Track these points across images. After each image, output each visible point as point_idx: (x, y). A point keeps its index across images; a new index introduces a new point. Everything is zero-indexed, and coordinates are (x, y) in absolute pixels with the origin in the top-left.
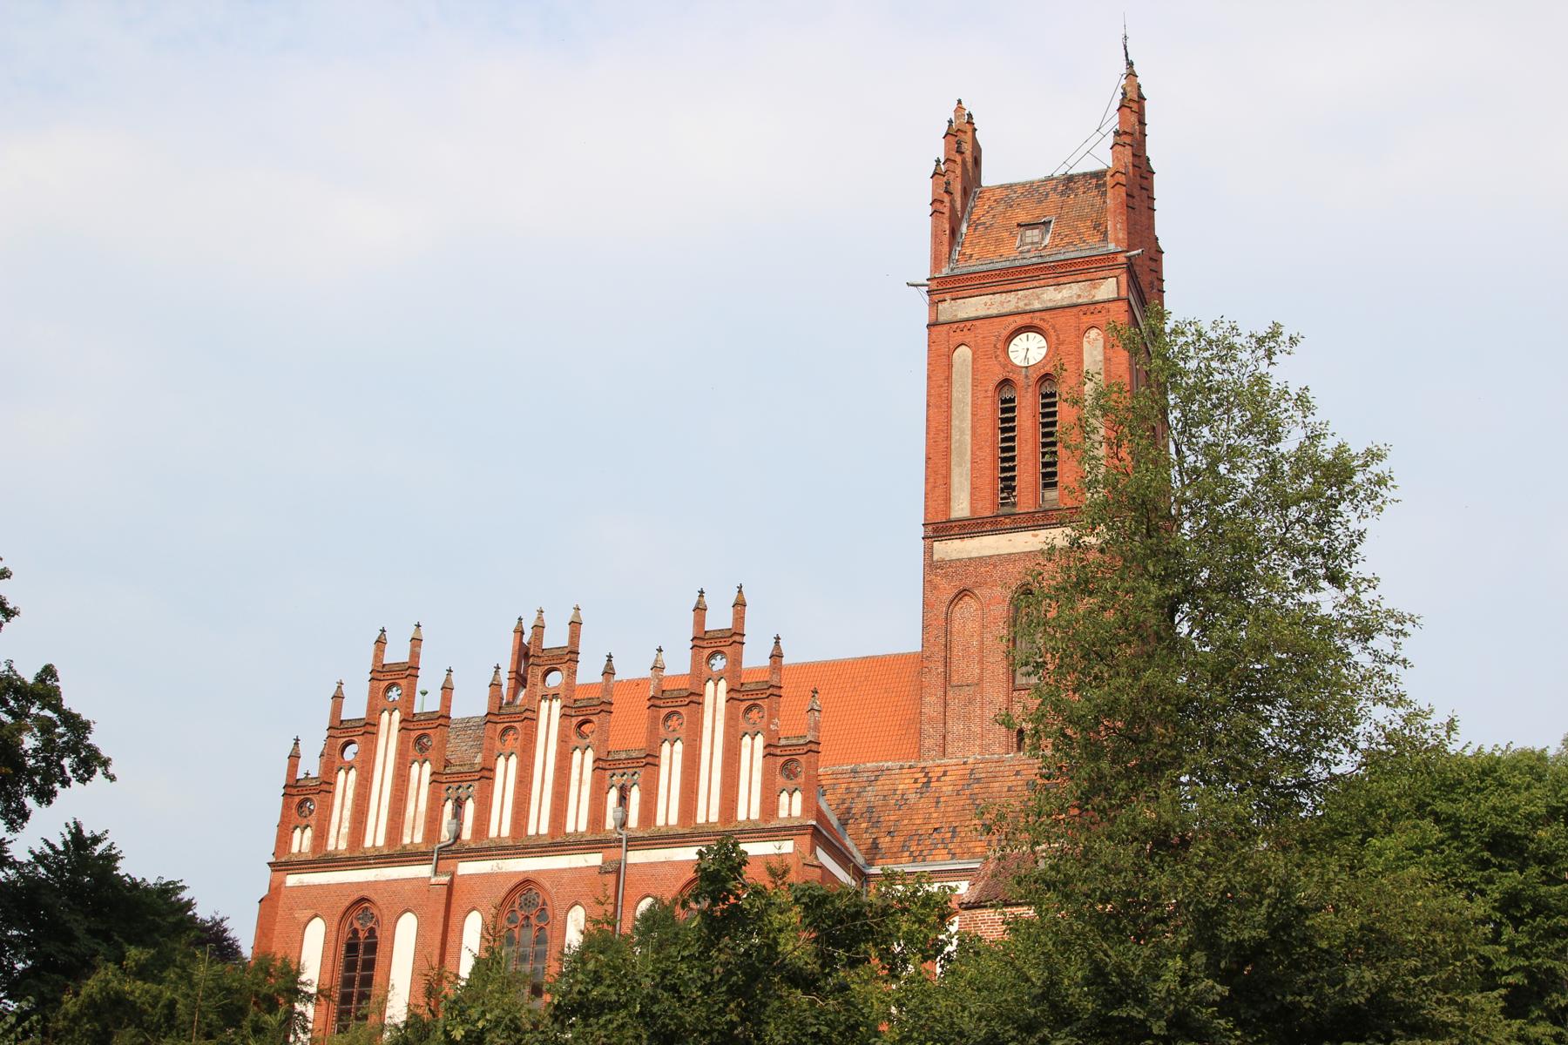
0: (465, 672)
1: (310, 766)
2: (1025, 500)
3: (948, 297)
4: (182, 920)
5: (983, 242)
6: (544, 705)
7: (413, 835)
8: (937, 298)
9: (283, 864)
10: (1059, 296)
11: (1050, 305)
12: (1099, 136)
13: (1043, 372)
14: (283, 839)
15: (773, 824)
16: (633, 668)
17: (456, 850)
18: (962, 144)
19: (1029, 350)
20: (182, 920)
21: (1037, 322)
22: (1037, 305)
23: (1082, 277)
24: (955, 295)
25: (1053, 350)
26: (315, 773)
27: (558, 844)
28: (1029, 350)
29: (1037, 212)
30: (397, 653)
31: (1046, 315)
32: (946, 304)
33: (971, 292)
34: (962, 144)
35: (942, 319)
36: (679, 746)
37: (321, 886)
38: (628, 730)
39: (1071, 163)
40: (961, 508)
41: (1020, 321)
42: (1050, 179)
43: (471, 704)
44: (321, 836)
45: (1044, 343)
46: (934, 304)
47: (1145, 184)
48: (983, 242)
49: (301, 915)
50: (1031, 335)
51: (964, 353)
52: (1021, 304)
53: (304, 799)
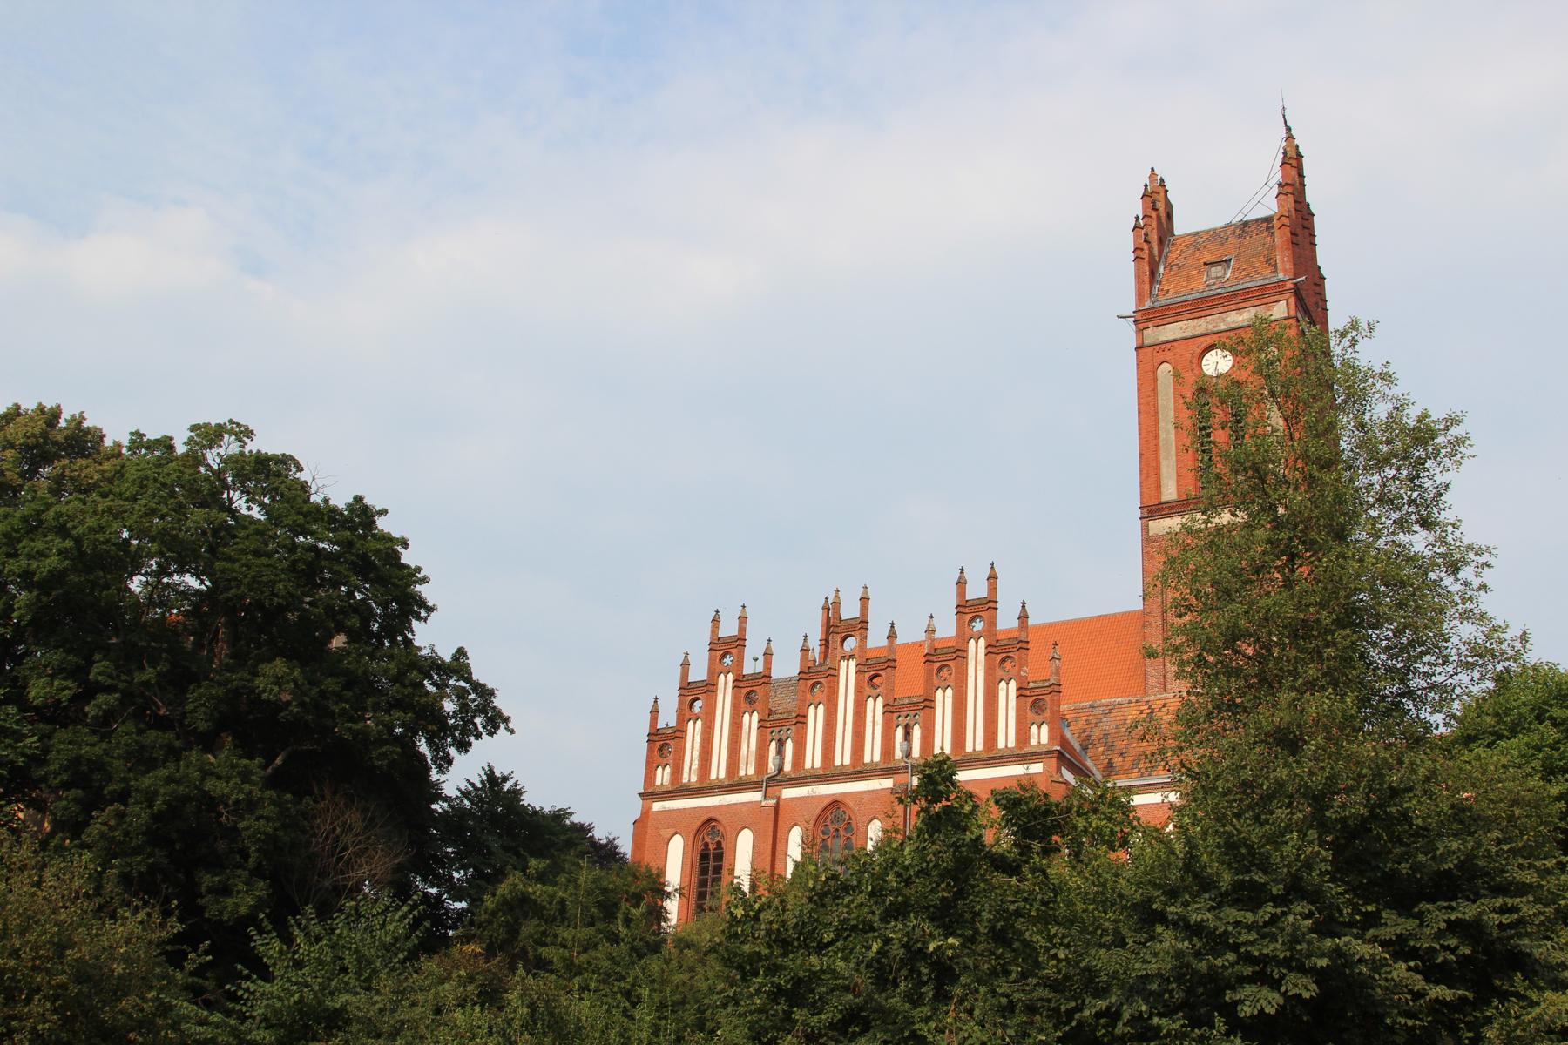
0: (783, 641)
1: (668, 718)
6: (843, 664)
7: (747, 769)
9: (649, 795)
13: (712, 815)
15: (1026, 750)
16: (911, 633)
22: (1223, 327)
26: (704, 677)
30: (728, 629)
35: (1146, 342)
36: (949, 692)
37: (679, 810)
38: (908, 681)
40: (1170, 492)
41: (1209, 340)
43: (786, 667)
44: (677, 772)
46: (1140, 331)
49: (665, 833)
53: (663, 743)
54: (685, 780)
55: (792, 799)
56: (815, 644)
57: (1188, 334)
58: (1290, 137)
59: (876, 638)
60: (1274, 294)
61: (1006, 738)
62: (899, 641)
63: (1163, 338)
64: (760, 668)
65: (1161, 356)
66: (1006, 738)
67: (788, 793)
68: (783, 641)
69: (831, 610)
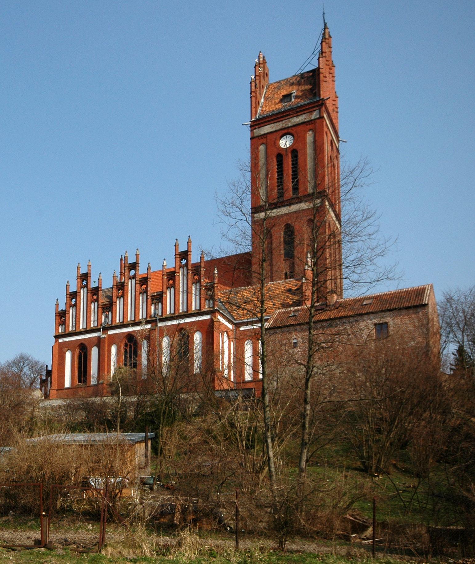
0: (105, 277)
2: (289, 194)
3: (257, 127)
4: (348, 536)
5: (270, 104)
8: (253, 128)
9: (57, 337)
10: (298, 120)
11: (295, 124)
12: (313, 55)
13: (292, 149)
14: (57, 329)
15: (78, 331)
16: (156, 267)
17: (106, 329)
18: (262, 63)
19: (285, 143)
20: (348, 536)
21: (290, 131)
22: (290, 125)
23: (307, 111)
24: (260, 126)
25: (295, 141)
27: (136, 323)
28: (285, 143)
29: (290, 90)
31: (293, 128)
32: (257, 130)
33: (264, 125)
34: (262, 63)
35: (255, 135)
37: (69, 341)
38: (153, 288)
39: (302, 68)
42: (294, 76)
43: (107, 284)
45: (292, 138)
46: (252, 131)
47: (331, 71)
48: (270, 104)
50: (288, 136)
51: (262, 148)
52: (284, 125)
53: (62, 316)
54: (70, 330)
55: (112, 334)
56: (118, 274)
57: (274, 129)
58: (325, 27)
59: (142, 271)
60: (312, 107)
62: (152, 271)
63: (262, 133)
64: (96, 285)
65: (261, 141)
67: (111, 332)
68: (105, 277)
69: (123, 259)
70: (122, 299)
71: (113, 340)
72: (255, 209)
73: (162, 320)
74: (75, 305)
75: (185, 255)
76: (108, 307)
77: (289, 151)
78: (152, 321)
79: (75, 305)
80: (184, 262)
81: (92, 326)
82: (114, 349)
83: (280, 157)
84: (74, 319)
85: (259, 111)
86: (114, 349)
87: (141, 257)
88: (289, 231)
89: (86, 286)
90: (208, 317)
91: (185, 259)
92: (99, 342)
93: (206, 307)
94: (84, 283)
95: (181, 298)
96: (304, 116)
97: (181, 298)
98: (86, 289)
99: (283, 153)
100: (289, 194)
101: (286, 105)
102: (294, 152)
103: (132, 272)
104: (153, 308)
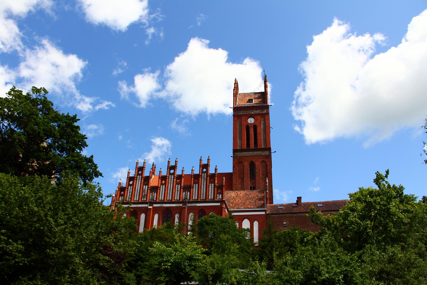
2: (252, 146)
16: (188, 172)
18: (236, 84)
19: (251, 121)
28: (251, 121)
61: (211, 197)
66: (211, 197)
67: (155, 205)
70: (164, 186)
71: (191, 209)
72: (235, 151)
73: (189, 202)
74: (132, 185)
75: (206, 166)
76: (188, 188)
77: (253, 125)
78: (184, 202)
79: (132, 185)
80: (205, 170)
81: (202, 198)
82: (156, 216)
83: (248, 127)
84: (130, 194)
85: (237, 104)
86: (156, 216)
87: (178, 163)
88: (252, 165)
89: (142, 174)
90: (219, 204)
91: (206, 168)
92: (180, 211)
93: (218, 198)
94: (140, 172)
95: (203, 191)
96: (259, 111)
97: (203, 191)
98: (141, 176)
99: (250, 126)
100: (252, 146)
101: (249, 104)
102: (255, 127)
103: (172, 171)
104: (184, 193)
